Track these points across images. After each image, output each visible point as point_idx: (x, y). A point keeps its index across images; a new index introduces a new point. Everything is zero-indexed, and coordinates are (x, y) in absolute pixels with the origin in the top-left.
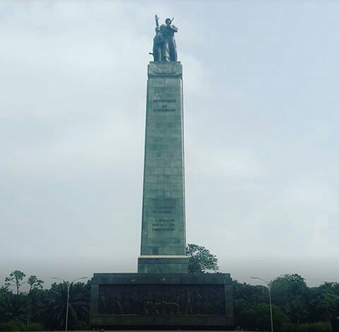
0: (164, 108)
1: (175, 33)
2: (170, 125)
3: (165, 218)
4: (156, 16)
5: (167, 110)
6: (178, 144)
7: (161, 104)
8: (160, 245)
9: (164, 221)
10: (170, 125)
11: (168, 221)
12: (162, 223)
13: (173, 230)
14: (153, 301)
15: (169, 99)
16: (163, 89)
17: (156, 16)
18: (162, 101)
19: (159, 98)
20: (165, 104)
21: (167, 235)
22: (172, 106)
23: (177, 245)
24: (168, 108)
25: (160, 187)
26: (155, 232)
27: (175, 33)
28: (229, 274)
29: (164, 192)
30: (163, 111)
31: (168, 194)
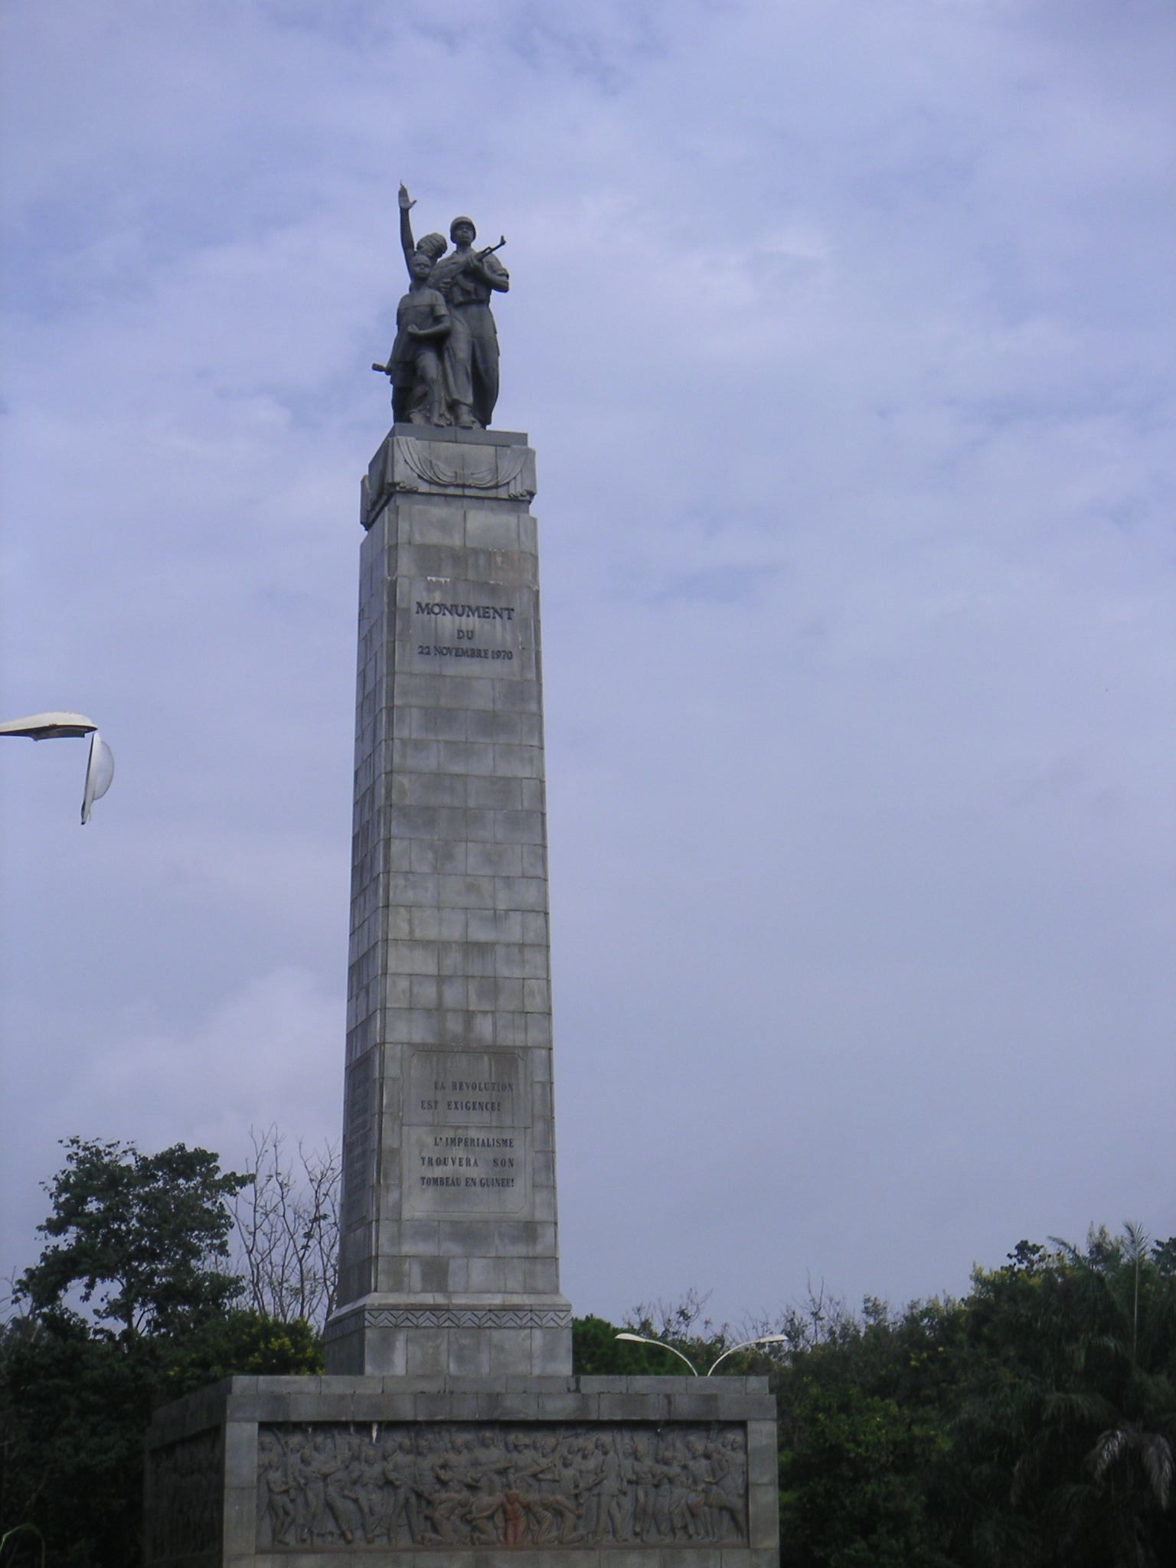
0: (466, 644)
1: (495, 295)
2: (491, 723)
3: (473, 1134)
4: (403, 193)
5: (476, 653)
6: (360, 738)
7: (448, 623)
8: (453, 1248)
9: (468, 1143)
10: (491, 723)
11: (485, 1144)
12: (459, 1152)
13: (505, 1183)
14: (385, 1458)
15: (485, 602)
16: (459, 558)
17: (403, 193)
18: (454, 610)
19: (437, 597)
20: (471, 622)
21: (482, 1206)
22: (496, 632)
23: (521, 1249)
24: (478, 644)
25: (452, 995)
26: (431, 1192)
27: (495, 295)
28: (182, 1148)
29: (469, 1016)
30: (460, 653)
31: (484, 1028)
